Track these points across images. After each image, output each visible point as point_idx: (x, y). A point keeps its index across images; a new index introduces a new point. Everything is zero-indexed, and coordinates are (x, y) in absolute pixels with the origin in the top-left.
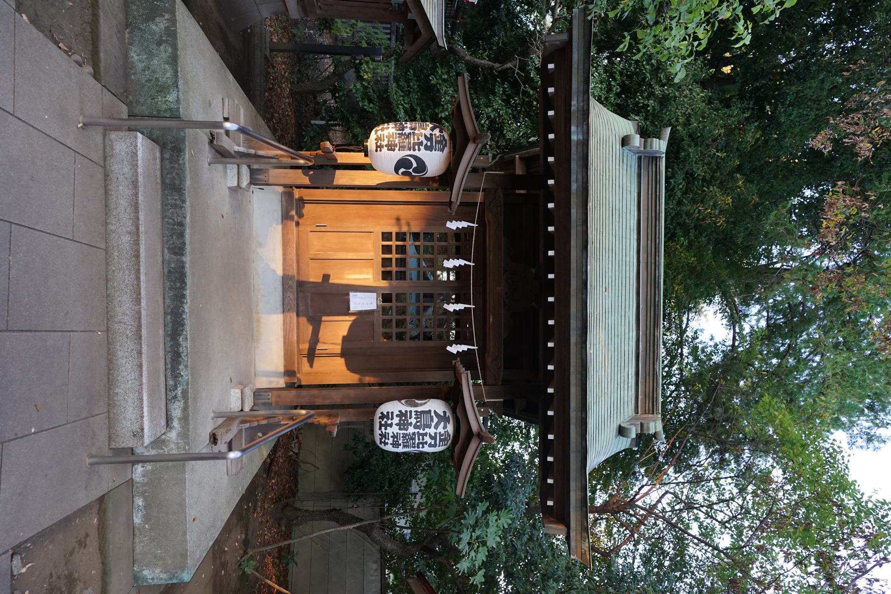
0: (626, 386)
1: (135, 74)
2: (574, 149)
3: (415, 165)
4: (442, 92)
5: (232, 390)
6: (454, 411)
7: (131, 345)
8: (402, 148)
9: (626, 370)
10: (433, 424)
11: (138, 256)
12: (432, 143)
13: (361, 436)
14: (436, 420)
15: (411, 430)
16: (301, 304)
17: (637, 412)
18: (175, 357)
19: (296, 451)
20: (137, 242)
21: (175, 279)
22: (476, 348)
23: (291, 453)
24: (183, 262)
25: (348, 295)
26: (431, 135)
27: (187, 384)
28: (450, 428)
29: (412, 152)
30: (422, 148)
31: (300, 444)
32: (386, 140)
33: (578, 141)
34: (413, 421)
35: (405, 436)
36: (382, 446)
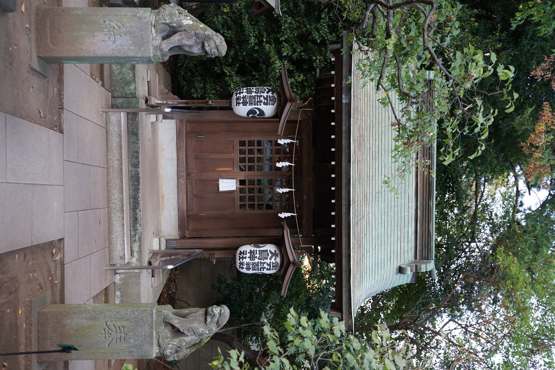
0: (406, 240)
1: (114, 76)
2: (344, 107)
3: (258, 113)
4: (282, 22)
5: (154, 239)
6: (281, 251)
7: (119, 214)
8: (251, 104)
9: (406, 229)
10: (269, 257)
11: (121, 171)
12: (267, 101)
13: (223, 279)
14: (270, 255)
15: (257, 260)
16: (188, 187)
17: (416, 258)
18: (135, 220)
19: (174, 291)
20: (121, 164)
21: (135, 180)
22: (296, 215)
23: (171, 292)
24: (138, 172)
25: (218, 181)
26: (267, 96)
27: (141, 234)
28: (278, 260)
29: (256, 106)
30: (262, 104)
31: (176, 286)
32: (242, 99)
33: (346, 103)
34: (258, 255)
35: (253, 264)
36: (241, 270)
